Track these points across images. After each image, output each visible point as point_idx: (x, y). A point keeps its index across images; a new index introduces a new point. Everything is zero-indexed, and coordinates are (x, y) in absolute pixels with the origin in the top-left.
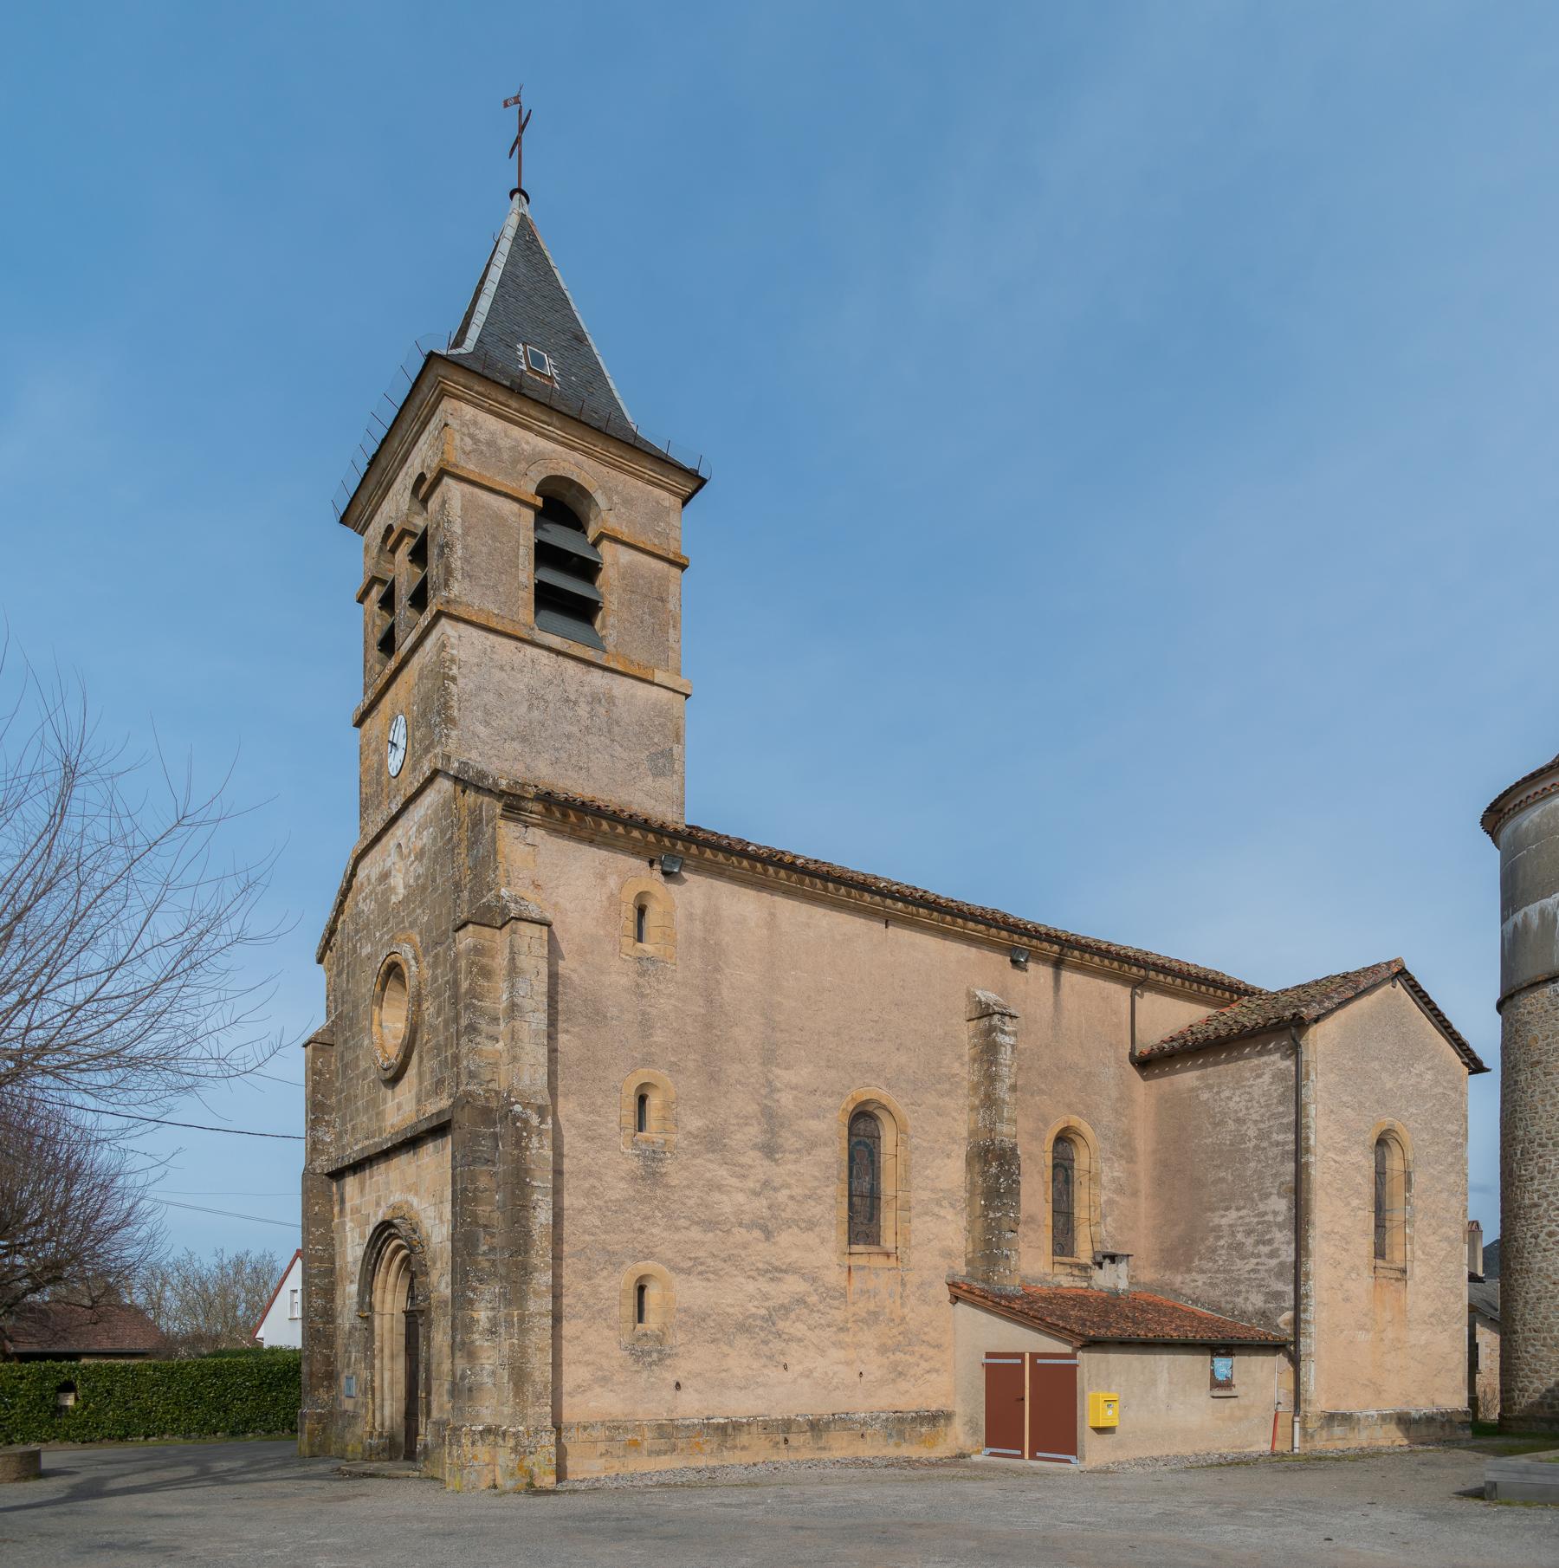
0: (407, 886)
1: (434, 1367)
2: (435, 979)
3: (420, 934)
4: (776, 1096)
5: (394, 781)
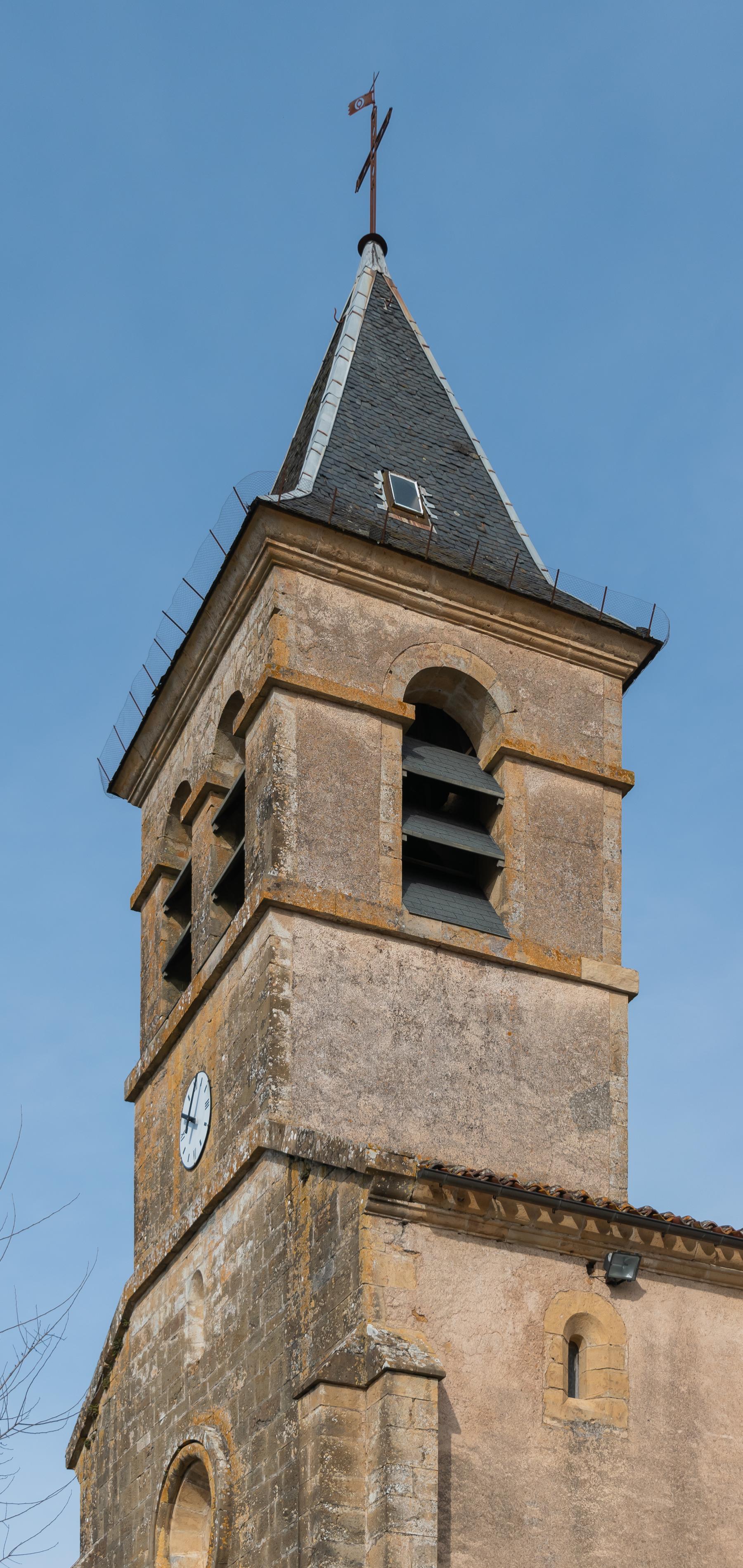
0: (210, 1336)
2: (255, 1477)
3: (232, 1408)
5: (190, 1176)
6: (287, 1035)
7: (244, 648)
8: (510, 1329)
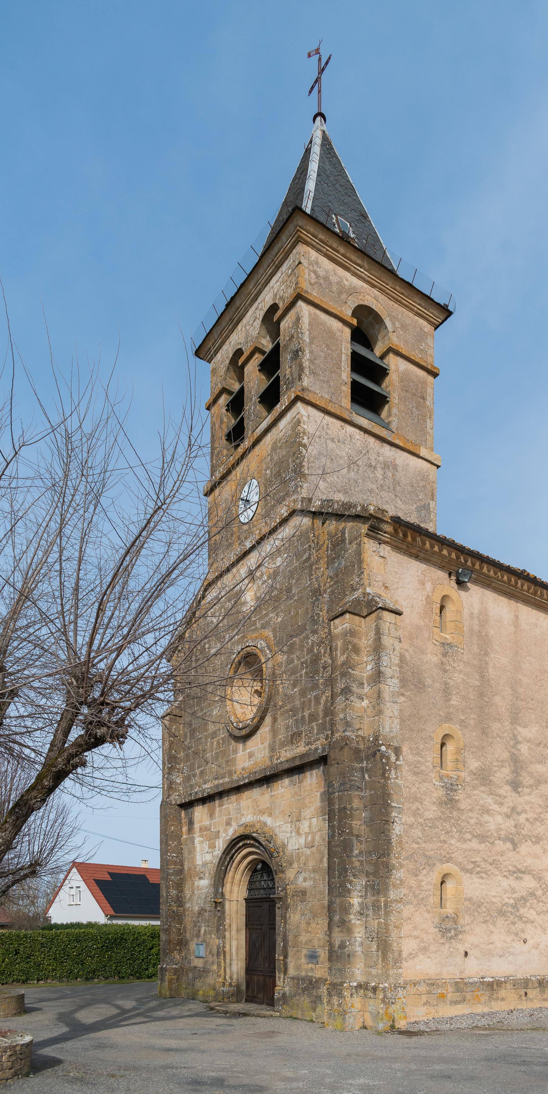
1: (290, 938)
2: (290, 661)
3: (274, 631)
4: (519, 747)
6: (306, 460)
7: (279, 283)
8: (420, 598)
